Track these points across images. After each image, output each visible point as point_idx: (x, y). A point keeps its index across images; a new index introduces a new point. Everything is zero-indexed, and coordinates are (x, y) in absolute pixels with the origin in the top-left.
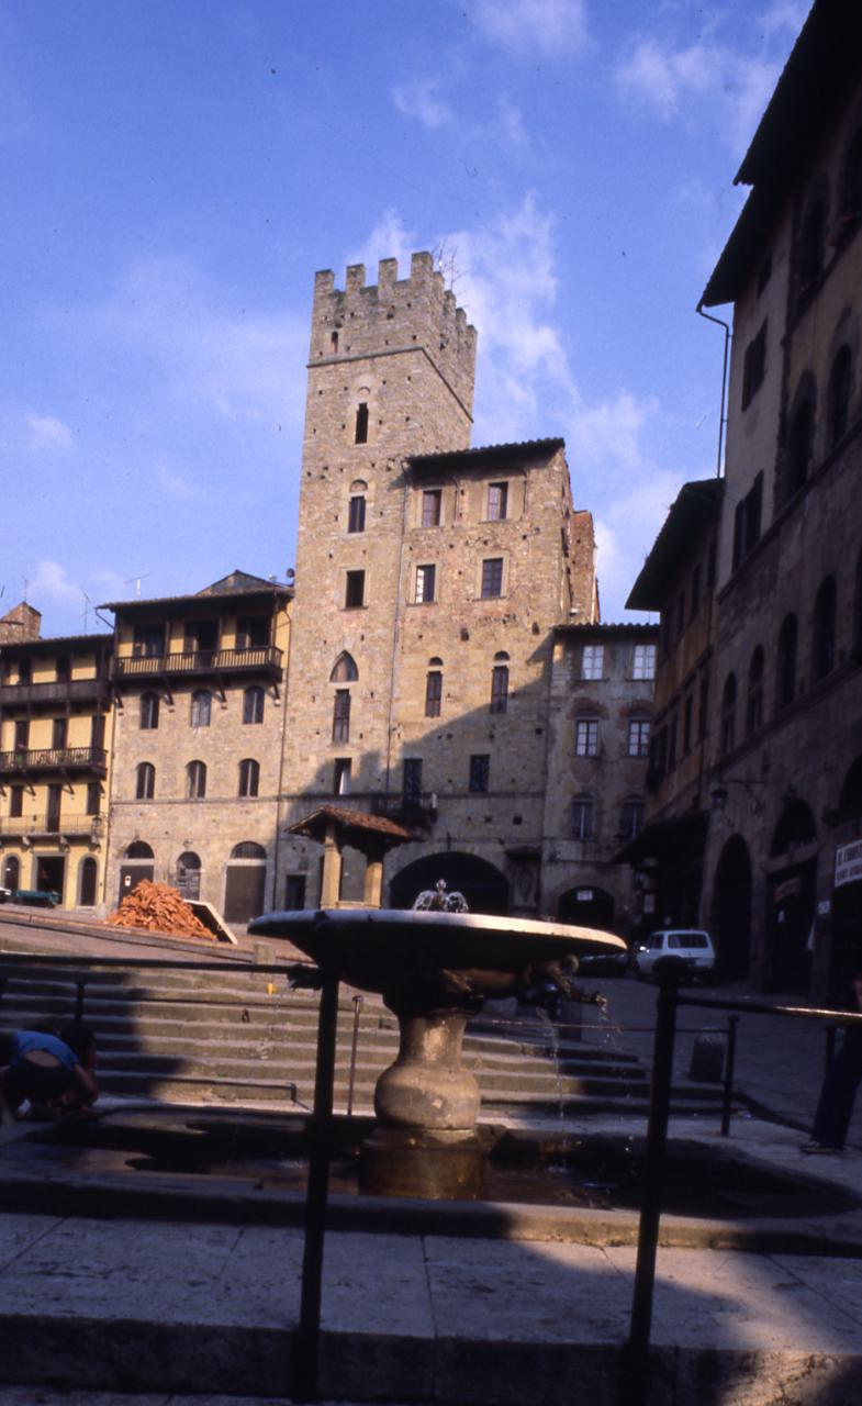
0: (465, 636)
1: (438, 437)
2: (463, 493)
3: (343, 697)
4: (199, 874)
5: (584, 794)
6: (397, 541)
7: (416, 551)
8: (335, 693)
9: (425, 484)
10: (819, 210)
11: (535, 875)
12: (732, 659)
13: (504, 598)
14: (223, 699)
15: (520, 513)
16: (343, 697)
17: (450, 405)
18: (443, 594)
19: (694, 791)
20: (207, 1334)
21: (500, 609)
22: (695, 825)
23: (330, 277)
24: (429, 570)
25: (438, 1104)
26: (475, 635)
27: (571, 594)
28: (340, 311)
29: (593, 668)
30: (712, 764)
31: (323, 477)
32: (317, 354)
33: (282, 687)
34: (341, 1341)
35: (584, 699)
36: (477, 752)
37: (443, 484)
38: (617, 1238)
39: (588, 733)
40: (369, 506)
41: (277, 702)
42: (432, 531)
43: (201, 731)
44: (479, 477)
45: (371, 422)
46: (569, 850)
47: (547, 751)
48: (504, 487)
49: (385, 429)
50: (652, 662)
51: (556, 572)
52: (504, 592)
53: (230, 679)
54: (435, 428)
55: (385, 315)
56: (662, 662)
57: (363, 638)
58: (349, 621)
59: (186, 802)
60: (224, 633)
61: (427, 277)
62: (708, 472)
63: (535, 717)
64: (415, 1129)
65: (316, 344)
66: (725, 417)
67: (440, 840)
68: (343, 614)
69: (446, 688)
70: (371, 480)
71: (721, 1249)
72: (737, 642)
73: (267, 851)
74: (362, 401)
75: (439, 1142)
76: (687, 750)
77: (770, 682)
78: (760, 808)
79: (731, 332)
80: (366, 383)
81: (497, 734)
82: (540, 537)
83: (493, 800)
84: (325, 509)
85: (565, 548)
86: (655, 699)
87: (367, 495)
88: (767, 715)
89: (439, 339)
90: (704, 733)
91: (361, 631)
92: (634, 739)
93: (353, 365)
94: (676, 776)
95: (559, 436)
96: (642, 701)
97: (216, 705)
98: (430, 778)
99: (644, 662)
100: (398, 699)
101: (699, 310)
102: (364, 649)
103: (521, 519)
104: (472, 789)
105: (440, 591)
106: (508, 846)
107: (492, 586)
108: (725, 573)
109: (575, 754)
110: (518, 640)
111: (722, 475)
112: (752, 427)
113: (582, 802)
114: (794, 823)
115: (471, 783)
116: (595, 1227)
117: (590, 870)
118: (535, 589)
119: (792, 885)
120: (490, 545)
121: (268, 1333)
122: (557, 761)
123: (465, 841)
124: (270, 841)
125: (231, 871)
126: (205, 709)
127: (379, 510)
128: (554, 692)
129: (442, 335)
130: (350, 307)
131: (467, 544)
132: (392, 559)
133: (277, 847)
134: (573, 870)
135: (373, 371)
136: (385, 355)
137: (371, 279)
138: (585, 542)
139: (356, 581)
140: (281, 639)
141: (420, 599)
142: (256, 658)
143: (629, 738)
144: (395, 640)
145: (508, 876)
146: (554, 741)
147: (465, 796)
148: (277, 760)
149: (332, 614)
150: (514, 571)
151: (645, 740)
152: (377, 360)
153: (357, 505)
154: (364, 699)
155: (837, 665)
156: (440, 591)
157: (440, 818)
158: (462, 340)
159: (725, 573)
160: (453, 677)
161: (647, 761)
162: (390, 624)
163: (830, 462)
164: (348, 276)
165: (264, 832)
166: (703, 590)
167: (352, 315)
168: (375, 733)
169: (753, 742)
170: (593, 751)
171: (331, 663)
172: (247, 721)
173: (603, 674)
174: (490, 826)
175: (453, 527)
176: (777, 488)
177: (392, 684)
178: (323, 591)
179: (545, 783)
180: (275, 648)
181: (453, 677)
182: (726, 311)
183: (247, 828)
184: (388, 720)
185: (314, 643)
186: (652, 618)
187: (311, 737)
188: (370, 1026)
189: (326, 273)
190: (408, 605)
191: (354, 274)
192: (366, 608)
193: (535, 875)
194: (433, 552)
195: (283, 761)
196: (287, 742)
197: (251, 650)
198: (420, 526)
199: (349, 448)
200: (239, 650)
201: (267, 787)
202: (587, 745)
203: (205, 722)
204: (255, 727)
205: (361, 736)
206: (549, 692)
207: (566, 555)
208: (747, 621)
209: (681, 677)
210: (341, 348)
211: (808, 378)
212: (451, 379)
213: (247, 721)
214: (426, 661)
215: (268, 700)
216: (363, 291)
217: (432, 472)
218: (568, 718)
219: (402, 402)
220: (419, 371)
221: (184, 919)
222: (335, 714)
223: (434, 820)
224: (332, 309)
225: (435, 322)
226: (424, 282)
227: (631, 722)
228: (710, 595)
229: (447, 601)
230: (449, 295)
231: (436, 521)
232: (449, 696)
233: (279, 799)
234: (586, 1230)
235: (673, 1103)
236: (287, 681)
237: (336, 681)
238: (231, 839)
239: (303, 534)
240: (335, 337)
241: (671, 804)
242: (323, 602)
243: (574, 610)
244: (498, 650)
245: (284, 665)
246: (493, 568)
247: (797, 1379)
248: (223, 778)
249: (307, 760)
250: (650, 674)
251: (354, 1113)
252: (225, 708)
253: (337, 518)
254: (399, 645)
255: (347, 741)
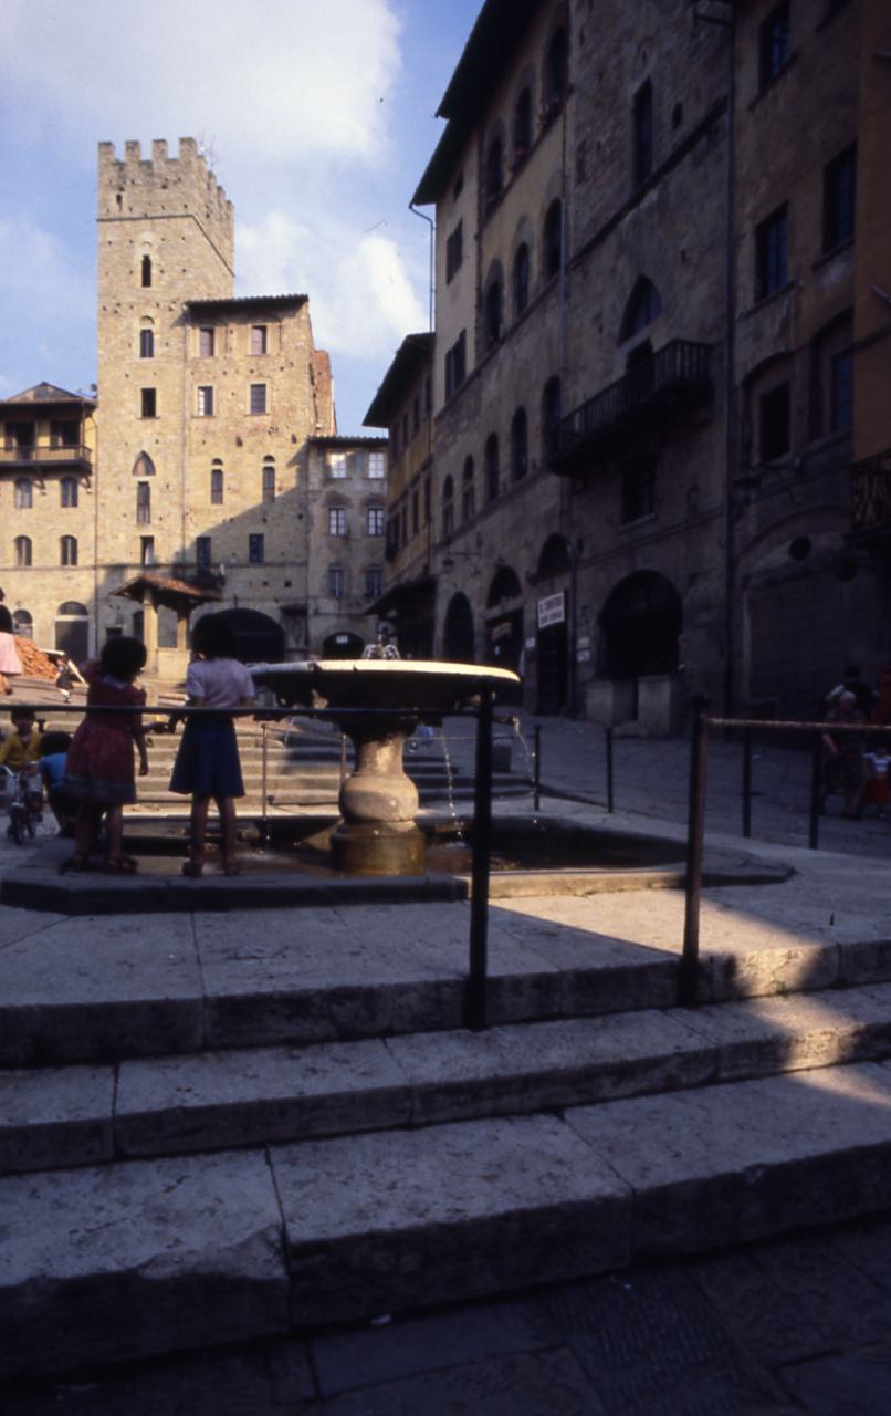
0: (239, 443)
1: (210, 287)
2: (232, 332)
3: (144, 488)
4: (31, 628)
5: (338, 563)
6: (180, 367)
7: (197, 375)
8: (137, 485)
9: (200, 323)
10: (497, 146)
11: (303, 625)
12: (448, 465)
13: (268, 415)
14: (43, 487)
15: (277, 350)
16: (144, 488)
17: (217, 263)
18: (221, 410)
19: (424, 561)
20: (402, 990)
21: (266, 423)
22: (425, 587)
23: (111, 148)
24: (208, 391)
25: (393, 803)
26: (247, 441)
27: (317, 413)
28: (123, 178)
29: (376, 470)
30: (437, 541)
31: (116, 312)
32: (105, 211)
33: (92, 479)
34: (498, 982)
35: (334, 493)
36: (255, 532)
37: (215, 324)
38: (589, 888)
39: (338, 518)
40: (156, 337)
41: (89, 490)
42: (209, 361)
43: (26, 512)
44: (244, 321)
45: (154, 271)
46: (328, 606)
47: (308, 532)
48: (264, 329)
49: (166, 277)
50: (381, 465)
51: (307, 396)
52: (268, 409)
53: (47, 471)
54: (206, 280)
55: (160, 186)
56: (394, 462)
57: (157, 442)
58: (145, 428)
59: (15, 569)
60: (40, 434)
61: (193, 159)
62: (422, 325)
63: (296, 506)
64: (375, 822)
65: (104, 202)
66: (434, 287)
67: (228, 600)
68: (140, 422)
69: (226, 483)
70: (156, 317)
71: (656, 889)
72: (452, 452)
73: (88, 608)
74: (146, 253)
75: (396, 831)
76: (416, 530)
77: (479, 480)
78: (477, 573)
79: (435, 226)
80: (147, 240)
81: (269, 519)
82: (293, 369)
83: (268, 568)
84: (120, 337)
85: (312, 379)
86: (382, 489)
87: (154, 328)
88: (478, 506)
89: (205, 209)
90: (429, 518)
91: (155, 437)
92: (372, 522)
93: (136, 223)
94: (408, 549)
95: (304, 293)
96: (376, 495)
97: (36, 491)
98: (217, 553)
99: (377, 465)
100: (189, 491)
101: (411, 207)
102: (159, 451)
103: (279, 355)
104: (251, 560)
105: (218, 405)
106: (282, 604)
107: (259, 404)
108: (439, 402)
109: (328, 533)
110: (281, 447)
111: (433, 330)
112: (455, 296)
113: (336, 570)
114: (504, 583)
115: (251, 557)
116: (575, 882)
117: (344, 621)
118: (292, 409)
119: (506, 627)
120: (256, 373)
121: (447, 984)
122: (316, 539)
123: (248, 600)
124: (90, 601)
125: (59, 625)
126: (27, 495)
127: (165, 341)
128: (311, 487)
129: (207, 207)
130: (130, 175)
131: (237, 372)
132: (178, 381)
133: (96, 607)
134: (333, 621)
135: (153, 230)
136: (163, 217)
137: (147, 153)
138: (324, 374)
139: (149, 397)
140: (89, 440)
141: (202, 413)
142: (67, 455)
143: (368, 522)
144: (184, 444)
145: (283, 626)
146: (313, 524)
147: (247, 566)
148: (92, 536)
149: (131, 422)
150: (275, 394)
151: (380, 523)
152: (156, 221)
153: (147, 337)
154: (162, 491)
155: (530, 471)
156: (218, 405)
157: (228, 582)
158: (223, 212)
159: (439, 402)
160: (231, 474)
161: (384, 538)
162: (179, 431)
163: (516, 327)
164: (127, 150)
165: (84, 595)
166: (423, 415)
167: (133, 182)
168: (172, 517)
169: (468, 525)
170: (342, 531)
171: (132, 461)
172: (64, 505)
173: (347, 473)
174: (268, 589)
175: (225, 358)
176: (477, 342)
177: (183, 478)
178: (122, 404)
179: (307, 555)
180: (84, 448)
181: (231, 474)
182: (430, 209)
183: (70, 591)
184: (182, 506)
185: (117, 444)
186: (382, 433)
187: (119, 519)
188: (249, 746)
189: (108, 144)
190: (193, 417)
191: (132, 148)
192: (159, 418)
193: (303, 625)
194: (210, 376)
195: (97, 537)
196: (100, 522)
197: (64, 448)
198: (198, 355)
199: (137, 290)
200: (53, 447)
201: (84, 557)
202: (338, 526)
203: (27, 504)
204: (71, 510)
205: (161, 519)
206: (307, 487)
207: (313, 383)
208: (459, 437)
209: (408, 477)
210: (125, 208)
211: (496, 266)
212: (216, 242)
213: (64, 505)
214: (210, 462)
215: (81, 490)
216: (141, 163)
217: (207, 315)
218: (323, 506)
219: (179, 257)
220: (191, 233)
221: (42, 665)
222: (138, 501)
223: (223, 584)
224: (115, 174)
225: (201, 195)
226: (190, 162)
227: (369, 510)
228: (429, 416)
229: (223, 415)
230: (211, 175)
231: (212, 353)
232: (229, 489)
233: (95, 568)
234: (569, 885)
235: (472, 790)
236: (96, 474)
237: (138, 475)
238: (58, 600)
239: (102, 357)
240: (119, 199)
241: (405, 571)
242: (123, 412)
243: (319, 425)
244: (266, 454)
245: (93, 460)
246: (259, 392)
247: (781, 967)
248: (47, 551)
249: (117, 537)
250: (381, 474)
251: (268, 814)
252: (44, 494)
253: (130, 345)
254: (187, 449)
255: (149, 522)
